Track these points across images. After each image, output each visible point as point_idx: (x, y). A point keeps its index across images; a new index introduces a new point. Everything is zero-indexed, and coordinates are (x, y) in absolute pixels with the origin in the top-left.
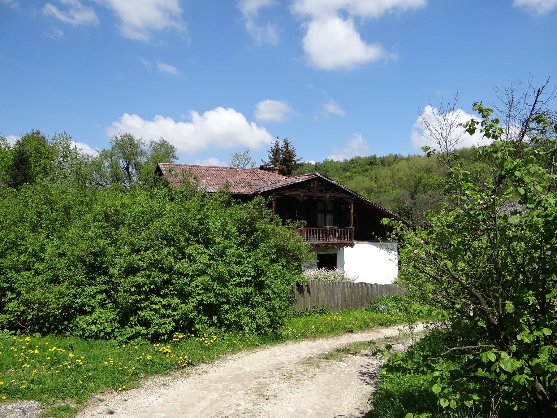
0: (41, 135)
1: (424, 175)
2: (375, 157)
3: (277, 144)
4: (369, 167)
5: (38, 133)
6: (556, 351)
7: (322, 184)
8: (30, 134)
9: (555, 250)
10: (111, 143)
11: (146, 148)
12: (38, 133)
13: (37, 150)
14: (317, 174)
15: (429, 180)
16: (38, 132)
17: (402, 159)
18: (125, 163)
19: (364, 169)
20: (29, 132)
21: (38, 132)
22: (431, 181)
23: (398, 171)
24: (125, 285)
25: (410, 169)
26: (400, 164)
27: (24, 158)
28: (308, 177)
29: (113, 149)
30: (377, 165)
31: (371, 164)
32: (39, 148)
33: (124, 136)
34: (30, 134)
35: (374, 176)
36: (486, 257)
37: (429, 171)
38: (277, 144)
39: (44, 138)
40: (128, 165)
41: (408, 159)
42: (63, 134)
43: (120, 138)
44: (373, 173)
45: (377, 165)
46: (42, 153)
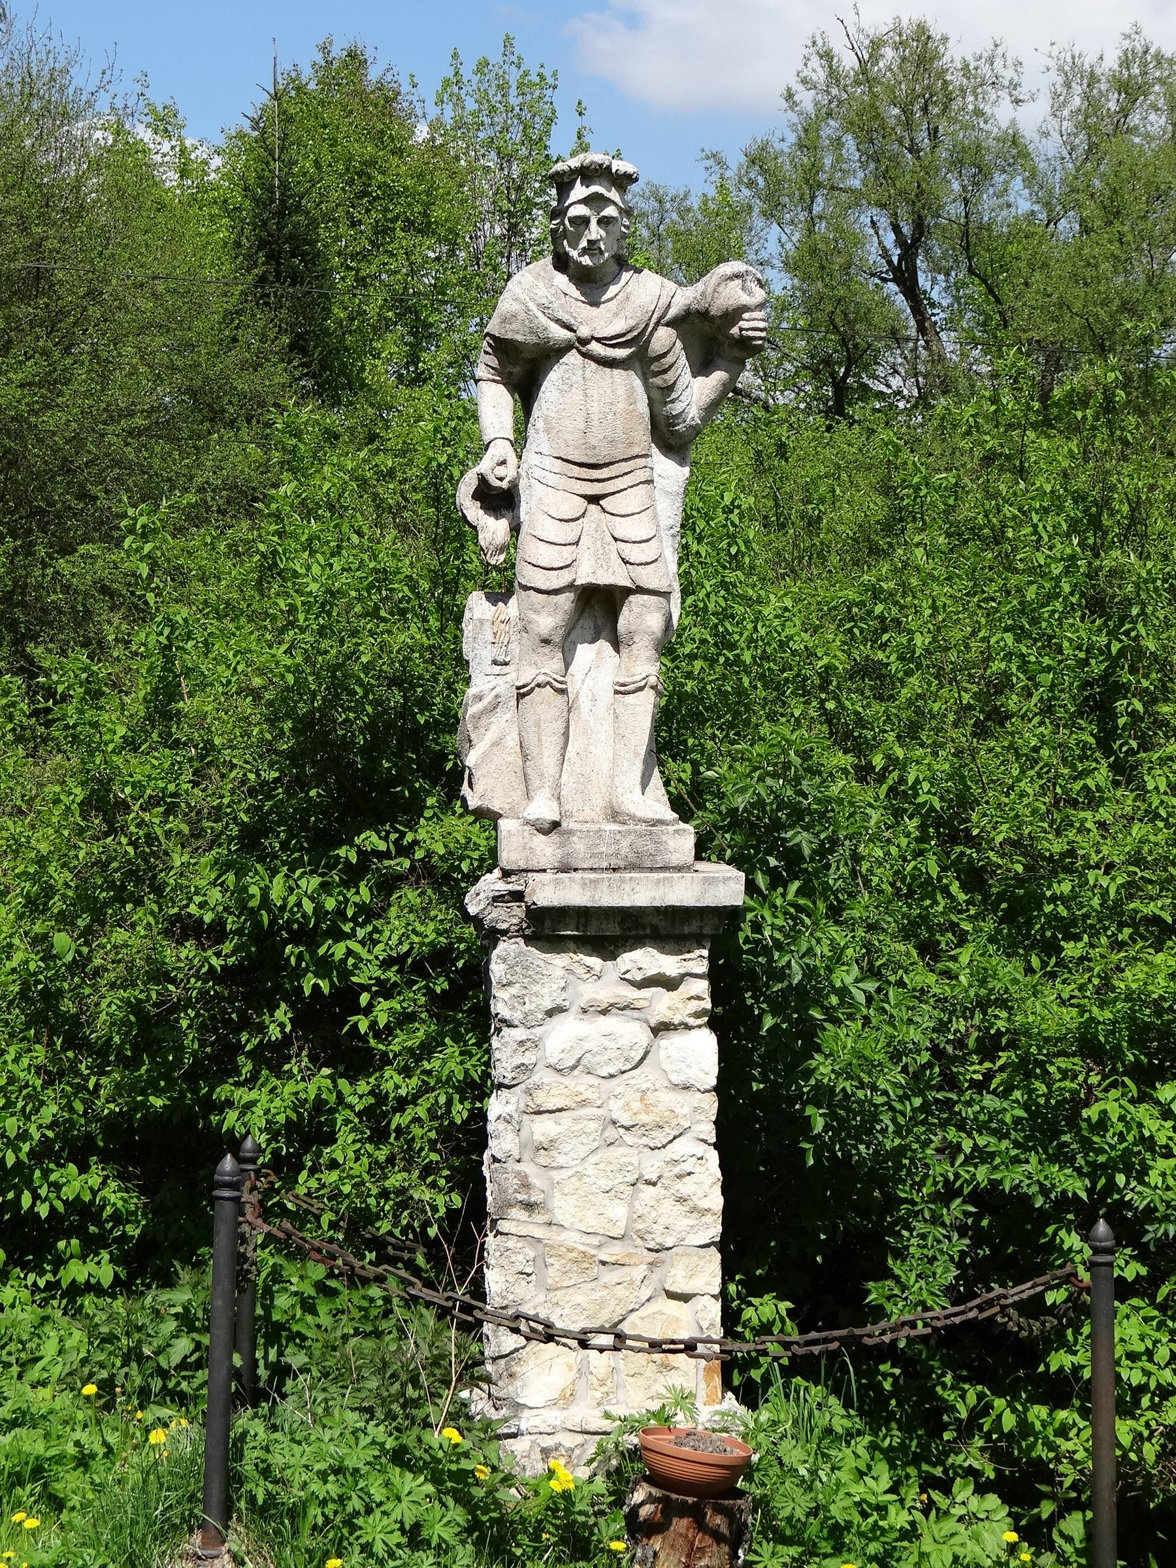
0: (374, 74)
5: (355, 60)
8: (307, 73)
9: (16, 848)
10: (789, 96)
11: (1033, 116)
12: (355, 60)
13: (362, 181)
16: (352, 55)
18: (890, 238)
20: (304, 61)
21: (352, 55)
24: (392, 1283)
27: (292, 238)
29: (808, 141)
32: (372, 163)
33: (876, 45)
34: (307, 73)
36: (934, 871)
39: (387, 99)
40: (909, 249)
42: (495, 57)
43: (848, 62)
46: (390, 193)
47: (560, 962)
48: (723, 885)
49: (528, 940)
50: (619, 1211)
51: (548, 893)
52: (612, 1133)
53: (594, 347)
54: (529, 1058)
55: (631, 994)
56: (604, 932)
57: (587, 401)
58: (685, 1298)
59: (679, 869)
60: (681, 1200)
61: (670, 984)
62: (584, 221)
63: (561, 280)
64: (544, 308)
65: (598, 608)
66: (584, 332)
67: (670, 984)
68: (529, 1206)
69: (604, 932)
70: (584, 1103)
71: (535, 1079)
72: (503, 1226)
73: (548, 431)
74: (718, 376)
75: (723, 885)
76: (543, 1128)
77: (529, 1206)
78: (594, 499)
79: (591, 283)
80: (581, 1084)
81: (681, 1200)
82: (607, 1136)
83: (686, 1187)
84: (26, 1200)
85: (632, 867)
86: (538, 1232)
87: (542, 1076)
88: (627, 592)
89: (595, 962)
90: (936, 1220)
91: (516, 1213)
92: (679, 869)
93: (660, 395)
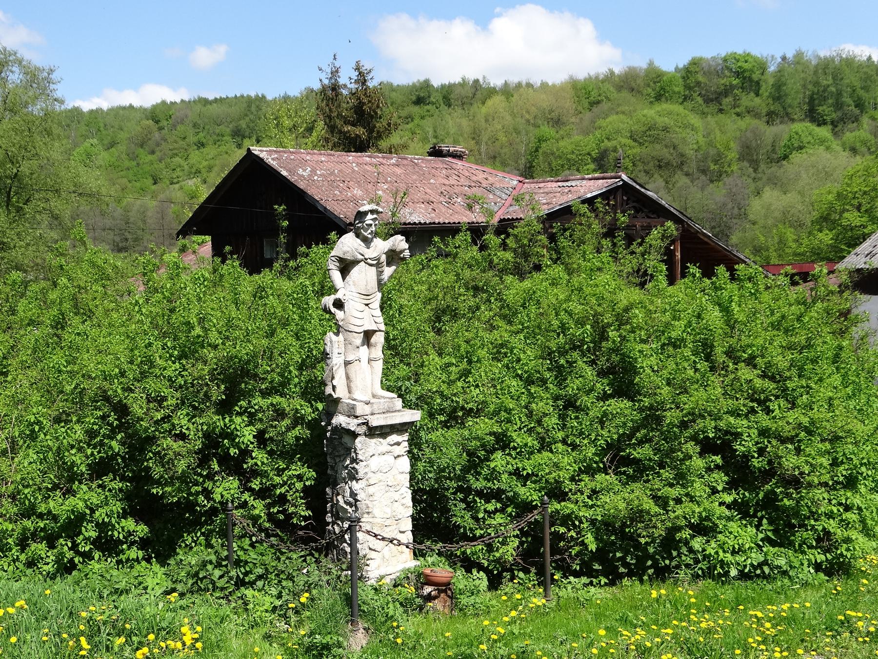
1: (547, 130)
2: (426, 84)
3: (335, 73)
4: (416, 110)
6: (2, 378)
7: (628, 199)
14: (624, 177)
15: (562, 143)
17: (492, 92)
19: (404, 113)
22: (566, 145)
23: (487, 121)
25: (513, 115)
26: (489, 103)
28: (611, 181)
30: (433, 103)
31: (419, 101)
35: (431, 133)
37: (557, 123)
38: (335, 73)
41: (507, 91)
44: (428, 124)
45: (433, 103)
47: (374, 441)
48: (414, 416)
49: (366, 436)
50: (388, 510)
51: (375, 422)
52: (387, 488)
53: (369, 261)
54: (366, 470)
55: (390, 448)
56: (382, 432)
57: (363, 277)
58: (403, 532)
59: (399, 411)
60: (403, 505)
61: (398, 444)
62: (371, 225)
63: (358, 241)
64: (356, 249)
65: (368, 335)
66: (367, 257)
67: (398, 444)
68: (368, 513)
69: (382, 432)
70: (380, 481)
71: (368, 476)
72: (362, 520)
73: (354, 285)
74: (394, 268)
75: (414, 416)
76: (371, 490)
77: (368, 513)
78: (367, 305)
79: (367, 241)
80: (379, 476)
81: (403, 505)
82: (382, 488)
83: (404, 501)
84: (116, 533)
85: (388, 412)
86: (371, 520)
87: (370, 475)
88: (376, 331)
89: (381, 440)
90: (455, 499)
91: (365, 515)
92: (399, 411)
93: (380, 273)
